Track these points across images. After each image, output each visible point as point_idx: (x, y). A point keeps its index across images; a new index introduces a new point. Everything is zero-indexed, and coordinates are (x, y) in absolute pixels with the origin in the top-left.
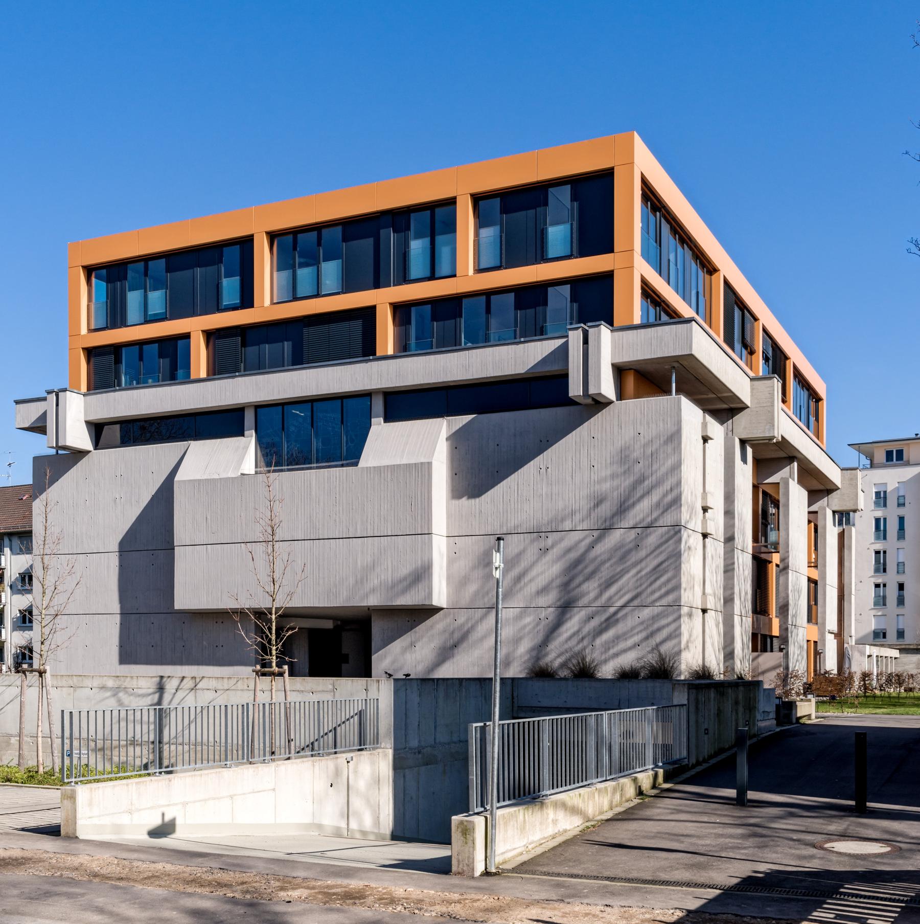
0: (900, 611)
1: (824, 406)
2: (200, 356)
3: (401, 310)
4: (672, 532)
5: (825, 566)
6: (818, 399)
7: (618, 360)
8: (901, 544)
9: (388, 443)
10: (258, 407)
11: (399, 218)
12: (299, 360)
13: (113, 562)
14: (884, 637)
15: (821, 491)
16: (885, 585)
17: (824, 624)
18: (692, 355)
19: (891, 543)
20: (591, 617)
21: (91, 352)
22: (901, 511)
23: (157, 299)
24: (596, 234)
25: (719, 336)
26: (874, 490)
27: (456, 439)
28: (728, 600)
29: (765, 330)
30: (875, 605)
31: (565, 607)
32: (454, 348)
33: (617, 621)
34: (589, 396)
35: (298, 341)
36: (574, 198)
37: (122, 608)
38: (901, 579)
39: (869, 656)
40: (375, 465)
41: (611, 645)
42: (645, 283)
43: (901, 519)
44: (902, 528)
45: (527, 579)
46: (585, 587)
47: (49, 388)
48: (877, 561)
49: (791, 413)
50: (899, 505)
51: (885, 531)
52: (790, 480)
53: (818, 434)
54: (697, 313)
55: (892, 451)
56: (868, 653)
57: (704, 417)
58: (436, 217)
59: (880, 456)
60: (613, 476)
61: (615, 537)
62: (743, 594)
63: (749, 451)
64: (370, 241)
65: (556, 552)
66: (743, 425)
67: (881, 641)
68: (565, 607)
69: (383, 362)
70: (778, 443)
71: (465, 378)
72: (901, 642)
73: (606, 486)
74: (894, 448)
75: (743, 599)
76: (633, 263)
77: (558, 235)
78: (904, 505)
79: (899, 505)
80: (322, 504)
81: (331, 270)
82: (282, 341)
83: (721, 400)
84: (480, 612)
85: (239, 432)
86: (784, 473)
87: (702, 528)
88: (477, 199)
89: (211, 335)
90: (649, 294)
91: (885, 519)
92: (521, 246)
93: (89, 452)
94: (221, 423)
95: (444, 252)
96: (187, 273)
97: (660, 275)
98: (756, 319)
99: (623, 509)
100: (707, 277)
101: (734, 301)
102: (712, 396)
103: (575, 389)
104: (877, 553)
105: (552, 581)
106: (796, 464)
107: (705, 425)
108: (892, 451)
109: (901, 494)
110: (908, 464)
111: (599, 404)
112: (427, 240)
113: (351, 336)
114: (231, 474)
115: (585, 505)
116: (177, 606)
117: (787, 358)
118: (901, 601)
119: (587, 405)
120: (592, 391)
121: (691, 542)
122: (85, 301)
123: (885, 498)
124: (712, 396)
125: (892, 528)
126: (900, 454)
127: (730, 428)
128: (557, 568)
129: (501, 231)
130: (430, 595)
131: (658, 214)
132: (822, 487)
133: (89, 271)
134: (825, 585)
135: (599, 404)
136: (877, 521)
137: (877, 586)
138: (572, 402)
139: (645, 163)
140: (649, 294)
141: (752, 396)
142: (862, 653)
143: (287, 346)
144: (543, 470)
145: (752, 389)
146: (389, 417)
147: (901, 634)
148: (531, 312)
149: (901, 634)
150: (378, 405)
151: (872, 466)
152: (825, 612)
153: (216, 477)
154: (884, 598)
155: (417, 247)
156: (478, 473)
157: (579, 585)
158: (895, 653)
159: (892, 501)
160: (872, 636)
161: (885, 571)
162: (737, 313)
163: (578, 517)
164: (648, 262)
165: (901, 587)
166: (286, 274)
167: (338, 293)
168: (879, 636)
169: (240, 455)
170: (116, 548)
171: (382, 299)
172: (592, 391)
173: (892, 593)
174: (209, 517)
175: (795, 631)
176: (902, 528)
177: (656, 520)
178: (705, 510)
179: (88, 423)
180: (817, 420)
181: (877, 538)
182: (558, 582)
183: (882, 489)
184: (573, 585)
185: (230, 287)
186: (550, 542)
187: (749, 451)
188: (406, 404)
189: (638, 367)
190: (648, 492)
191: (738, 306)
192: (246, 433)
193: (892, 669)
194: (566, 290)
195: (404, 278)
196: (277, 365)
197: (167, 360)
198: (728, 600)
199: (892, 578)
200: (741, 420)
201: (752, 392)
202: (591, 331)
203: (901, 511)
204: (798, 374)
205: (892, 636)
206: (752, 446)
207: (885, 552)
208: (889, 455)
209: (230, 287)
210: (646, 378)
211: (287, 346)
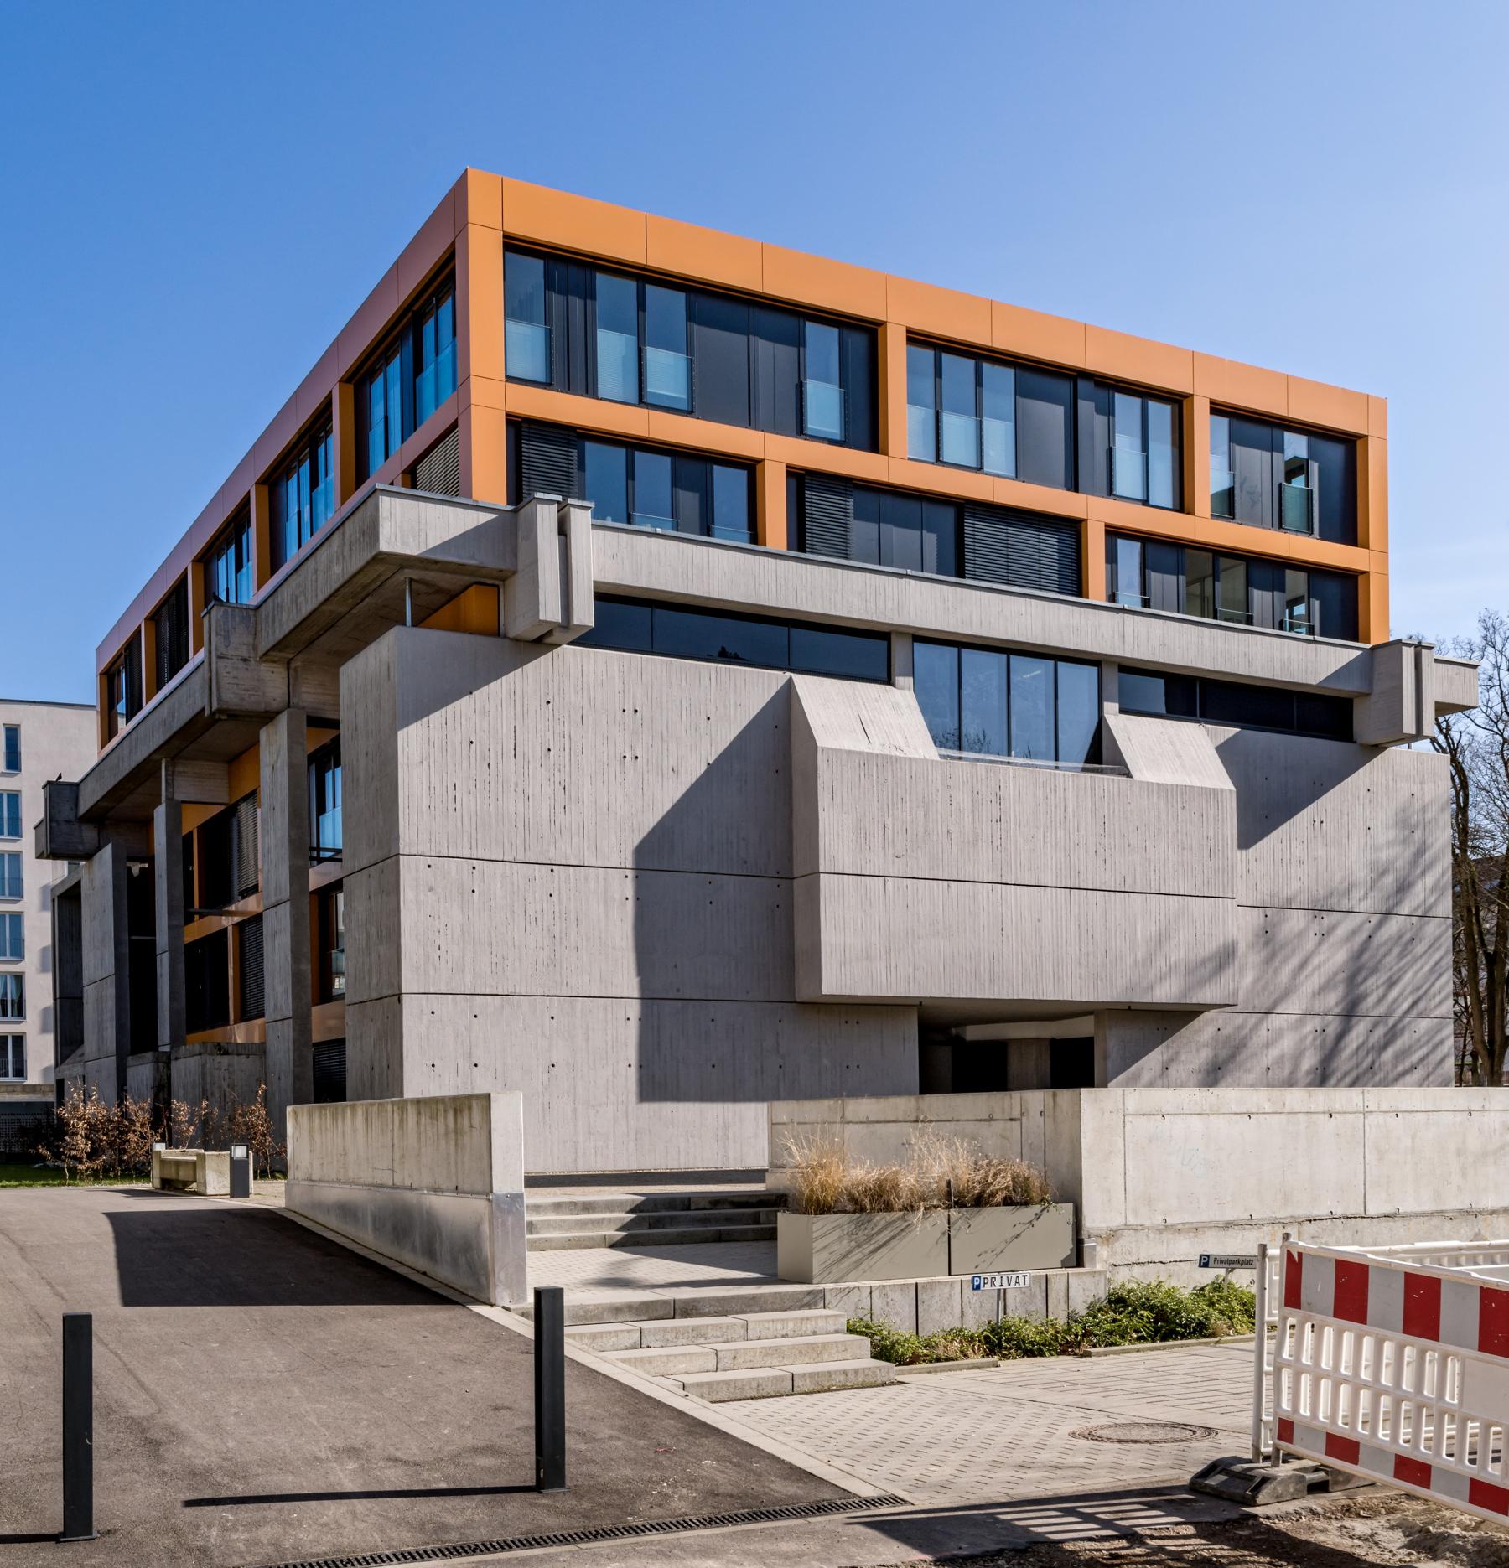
12: (956, 565)
13: (624, 887)
20: (1375, 1025)
31: (1349, 1013)
32: (920, 574)
33: (1403, 1030)
37: (643, 986)
41: (1109, 1044)
45: (1310, 968)
46: (1371, 981)
60: (1390, 844)
61: (1394, 926)
65: (1341, 932)
68: (1349, 1013)
69: (840, 571)
71: (960, 631)
73: (1384, 855)
80: (1083, 832)
84: (1253, 1019)
99: (1403, 888)
105: (1335, 974)
111: (541, 643)
115: (1362, 874)
128: (1341, 956)
129: (549, 334)
144: (1317, 824)
156: (1263, 811)
157: (1365, 979)
163: (1358, 894)
167: (832, 442)
170: (620, 851)
174: (889, 823)
177: (1430, 908)
182: (1342, 976)
184: (1360, 978)
186: (1326, 922)
190: (1429, 867)
196: (912, 566)
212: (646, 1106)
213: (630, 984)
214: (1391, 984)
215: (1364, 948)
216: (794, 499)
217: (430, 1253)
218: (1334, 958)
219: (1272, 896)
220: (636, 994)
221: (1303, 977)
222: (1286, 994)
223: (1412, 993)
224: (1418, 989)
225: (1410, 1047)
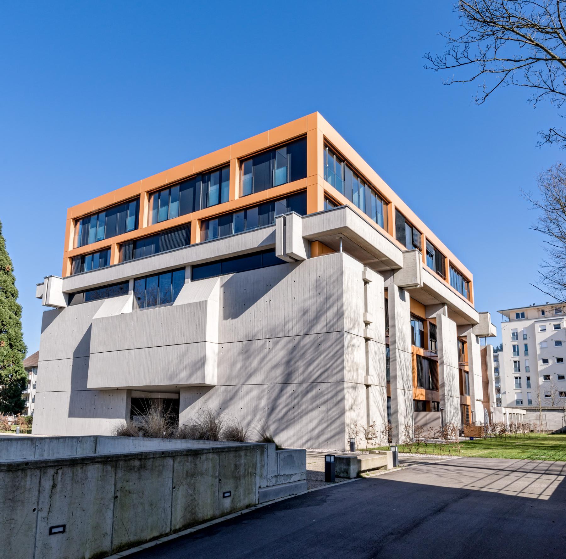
0: (529, 390)
1: (472, 285)
2: (115, 255)
3: (204, 222)
4: (339, 336)
5: (472, 364)
6: (468, 282)
7: (306, 234)
8: (527, 357)
9: (191, 291)
10: (136, 279)
11: (204, 176)
13: (70, 363)
14: (522, 403)
15: (469, 325)
16: (520, 378)
17: (473, 396)
18: (346, 227)
19: (521, 358)
21: (72, 259)
22: (526, 342)
23: (101, 230)
24: (299, 170)
25: (392, 236)
26: (511, 332)
27: (225, 286)
28: (390, 379)
29: (427, 239)
30: (516, 387)
34: (287, 255)
35: (156, 242)
36: (288, 152)
38: (528, 374)
39: (505, 414)
40: (181, 304)
42: (325, 192)
43: (526, 346)
44: (526, 350)
47: (45, 276)
48: (515, 366)
49: (449, 285)
50: (524, 339)
51: (518, 351)
52: (442, 316)
53: (469, 298)
54: (377, 222)
55: (519, 314)
56: (504, 412)
57: (365, 269)
58: (221, 172)
59: (513, 316)
60: (311, 298)
61: (308, 339)
62: (405, 377)
63: (407, 295)
64: (192, 189)
66: (399, 279)
67: (520, 405)
70: (421, 288)
72: (530, 406)
74: (520, 312)
75: (405, 379)
76: (319, 182)
77: (279, 173)
78: (527, 338)
79: (524, 339)
81: (174, 207)
82: (151, 244)
83: (383, 262)
85: (126, 292)
86: (441, 311)
87: (364, 334)
88: (242, 161)
89: (121, 245)
90: (327, 197)
91: (518, 346)
92: (262, 181)
93: (65, 307)
94: (117, 288)
95: (224, 190)
96: (114, 216)
97: (344, 195)
98: (421, 234)
100: (384, 206)
101: (402, 221)
102: (376, 260)
103: (279, 252)
104: (515, 362)
106: (446, 307)
107: (364, 273)
108: (519, 314)
109: (525, 333)
110: (527, 319)
112: (218, 185)
113: (180, 236)
114: (117, 314)
116: (89, 386)
117: (445, 257)
118: (529, 386)
119: (291, 263)
120: (288, 252)
121: (355, 341)
122: (73, 234)
123: (517, 336)
124: (376, 260)
125: (522, 350)
126: (523, 315)
127: (392, 280)
130: (204, 378)
131: (342, 163)
132: (468, 323)
133: (76, 220)
134: (473, 374)
135: (297, 261)
136: (514, 347)
137: (516, 378)
138: (279, 262)
139: (323, 129)
140: (327, 197)
141: (404, 261)
142: (501, 412)
143: (153, 246)
145: (404, 258)
146: (194, 278)
147: (530, 402)
148: (266, 215)
149: (530, 402)
150: (188, 272)
151: (510, 321)
152: (473, 390)
153: (110, 316)
154: (520, 384)
155: (213, 189)
156: (235, 306)
157: (296, 363)
158: (524, 412)
159: (520, 337)
160: (515, 403)
161: (519, 371)
162: (408, 229)
164: (334, 187)
165: (528, 378)
166: (155, 211)
168: (519, 402)
169: (126, 303)
171: (194, 217)
172: (287, 252)
173: (524, 381)
175: (450, 399)
176: (526, 350)
177: (333, 325)
178: (367, 324)
179: (64, 293)
180: (469, 291)
181: (514, 355)
183: (515, 332)
184: (293, 362)
185: (130, 220)
187: (407, 295)
188: (203, 270)
189: (320, 239)
191: (408, 224)
192: (129, 292)
193: (522, 421)
194: (284, 202)
195: (206, 206)
197: (103, 259)
198: (390, 379)
199: (523, 374)
200: (398, 275)
201: (404, 259)
202: (288, 217)
203: (526, 342)
204: (452, 266)
205: (525, 403)
206: (409, 291)
207: (519, 362)
208: (517, 316)
209: (130, 220)
210: (321, 244)
211: (153, 246)
212: (70, 419)
213: (69, 387)
214: (309, 364)
215: (295, 348)
216: (81, 290)
217: (122, 289)
218: (279, 353)
219: (246, 337)
220: (70, 390)
221: (263, 364)
222: (256, 371)
223: (286, 406)
224: (326, 365)
225: (322, 393)
